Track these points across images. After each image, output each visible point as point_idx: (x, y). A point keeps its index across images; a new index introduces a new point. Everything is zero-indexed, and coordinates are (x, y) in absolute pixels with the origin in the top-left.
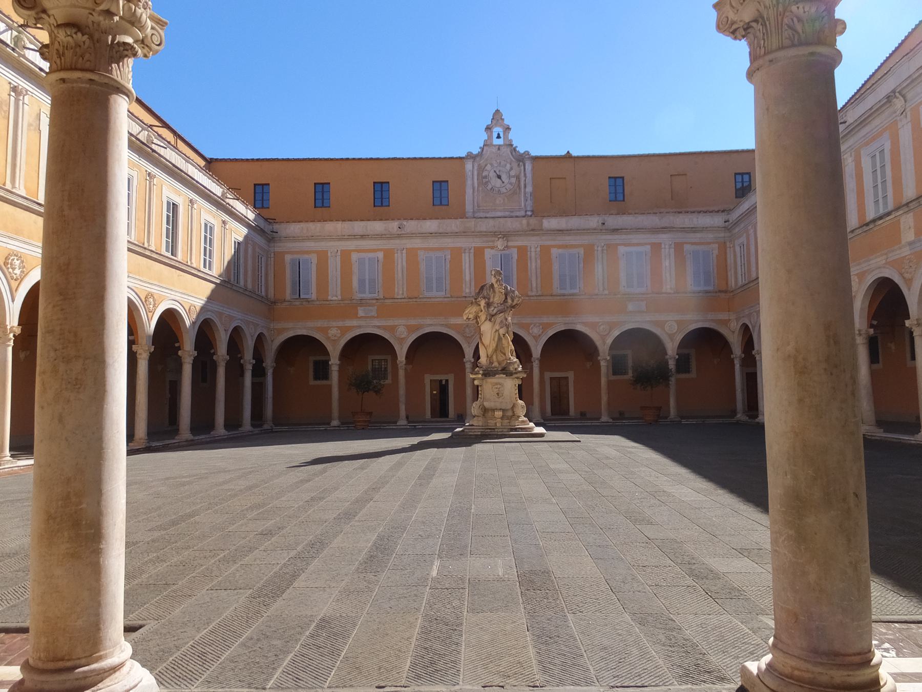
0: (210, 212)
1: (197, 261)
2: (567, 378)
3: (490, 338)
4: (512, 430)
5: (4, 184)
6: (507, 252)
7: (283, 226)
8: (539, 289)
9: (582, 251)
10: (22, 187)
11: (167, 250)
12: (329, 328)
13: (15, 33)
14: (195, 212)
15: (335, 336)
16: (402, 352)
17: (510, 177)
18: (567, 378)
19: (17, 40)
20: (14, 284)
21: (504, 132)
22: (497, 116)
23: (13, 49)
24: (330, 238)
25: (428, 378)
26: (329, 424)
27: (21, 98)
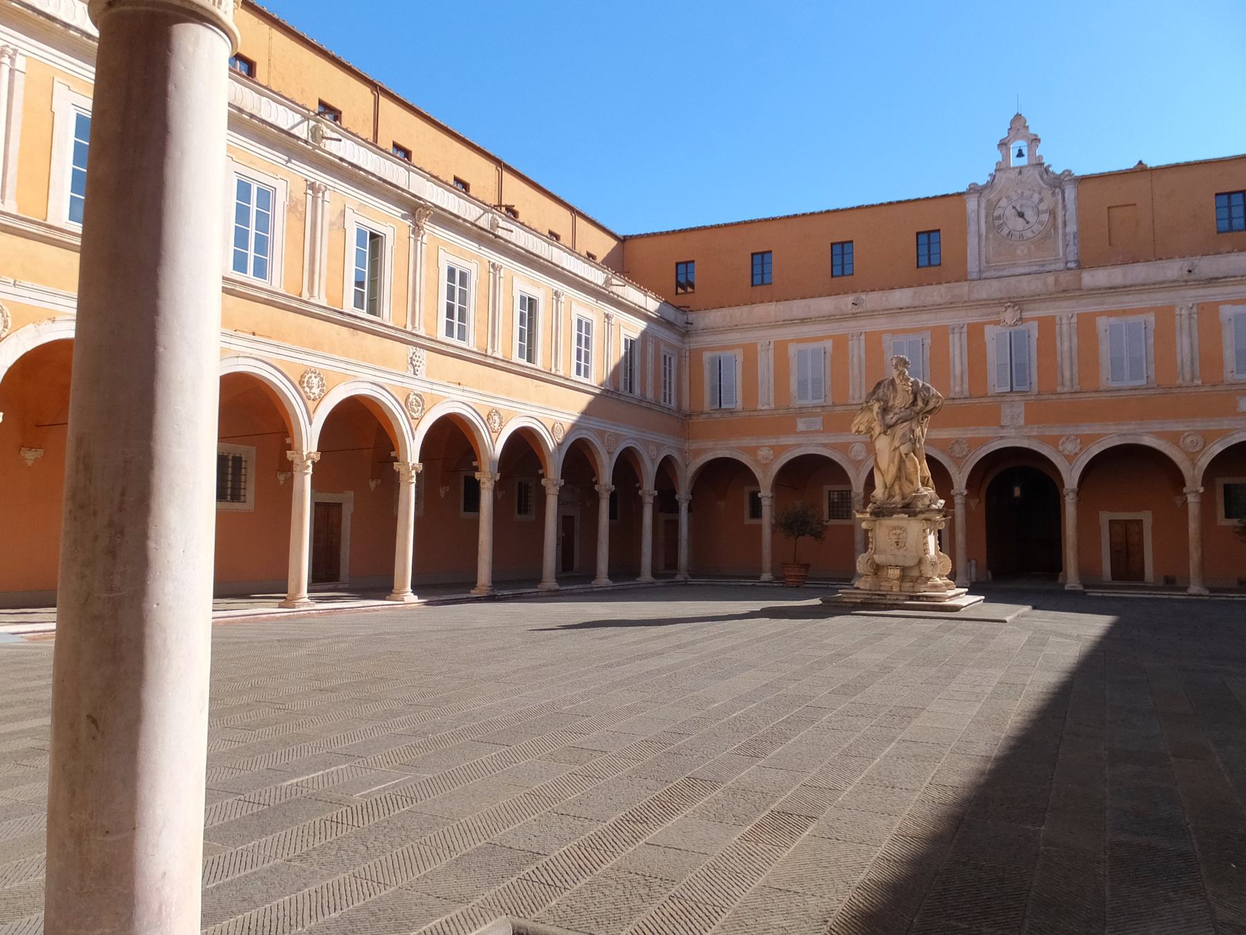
0: (586, 305)
1: (566, 366)
2: (1139, 522)
3: (884, 456)
4: (911, 598)
5: (300, 295)
6: (1021, 327)
7: (702, 313)
8: (1076, 381)
9: (1151, 318)
10: (323, 295)
11: (521, 356)
12: (758, 448)
13: (312, 123)
14: (562, 307)
15: (766, 459)
16: (1071, 478)
17: (1039, 213)
18: (1139, 522)
19: (314, 132)
20: (311, 405)
21: (1029, 147)
22: (1018, 124)
23: (306, 142)
24: (759, 326)
25: (1105, 517)
26: (758, 577)
27: (320, 195)
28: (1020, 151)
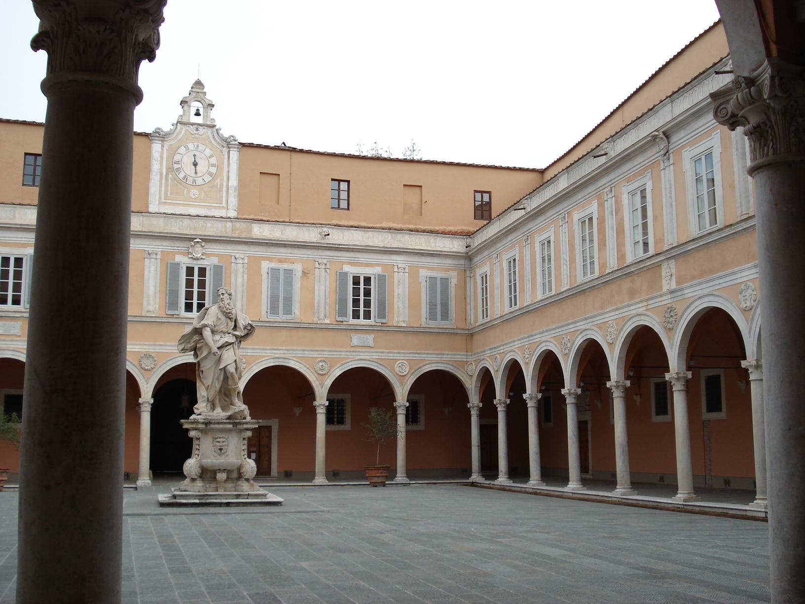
28: (198, 110)
